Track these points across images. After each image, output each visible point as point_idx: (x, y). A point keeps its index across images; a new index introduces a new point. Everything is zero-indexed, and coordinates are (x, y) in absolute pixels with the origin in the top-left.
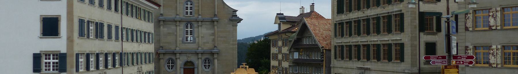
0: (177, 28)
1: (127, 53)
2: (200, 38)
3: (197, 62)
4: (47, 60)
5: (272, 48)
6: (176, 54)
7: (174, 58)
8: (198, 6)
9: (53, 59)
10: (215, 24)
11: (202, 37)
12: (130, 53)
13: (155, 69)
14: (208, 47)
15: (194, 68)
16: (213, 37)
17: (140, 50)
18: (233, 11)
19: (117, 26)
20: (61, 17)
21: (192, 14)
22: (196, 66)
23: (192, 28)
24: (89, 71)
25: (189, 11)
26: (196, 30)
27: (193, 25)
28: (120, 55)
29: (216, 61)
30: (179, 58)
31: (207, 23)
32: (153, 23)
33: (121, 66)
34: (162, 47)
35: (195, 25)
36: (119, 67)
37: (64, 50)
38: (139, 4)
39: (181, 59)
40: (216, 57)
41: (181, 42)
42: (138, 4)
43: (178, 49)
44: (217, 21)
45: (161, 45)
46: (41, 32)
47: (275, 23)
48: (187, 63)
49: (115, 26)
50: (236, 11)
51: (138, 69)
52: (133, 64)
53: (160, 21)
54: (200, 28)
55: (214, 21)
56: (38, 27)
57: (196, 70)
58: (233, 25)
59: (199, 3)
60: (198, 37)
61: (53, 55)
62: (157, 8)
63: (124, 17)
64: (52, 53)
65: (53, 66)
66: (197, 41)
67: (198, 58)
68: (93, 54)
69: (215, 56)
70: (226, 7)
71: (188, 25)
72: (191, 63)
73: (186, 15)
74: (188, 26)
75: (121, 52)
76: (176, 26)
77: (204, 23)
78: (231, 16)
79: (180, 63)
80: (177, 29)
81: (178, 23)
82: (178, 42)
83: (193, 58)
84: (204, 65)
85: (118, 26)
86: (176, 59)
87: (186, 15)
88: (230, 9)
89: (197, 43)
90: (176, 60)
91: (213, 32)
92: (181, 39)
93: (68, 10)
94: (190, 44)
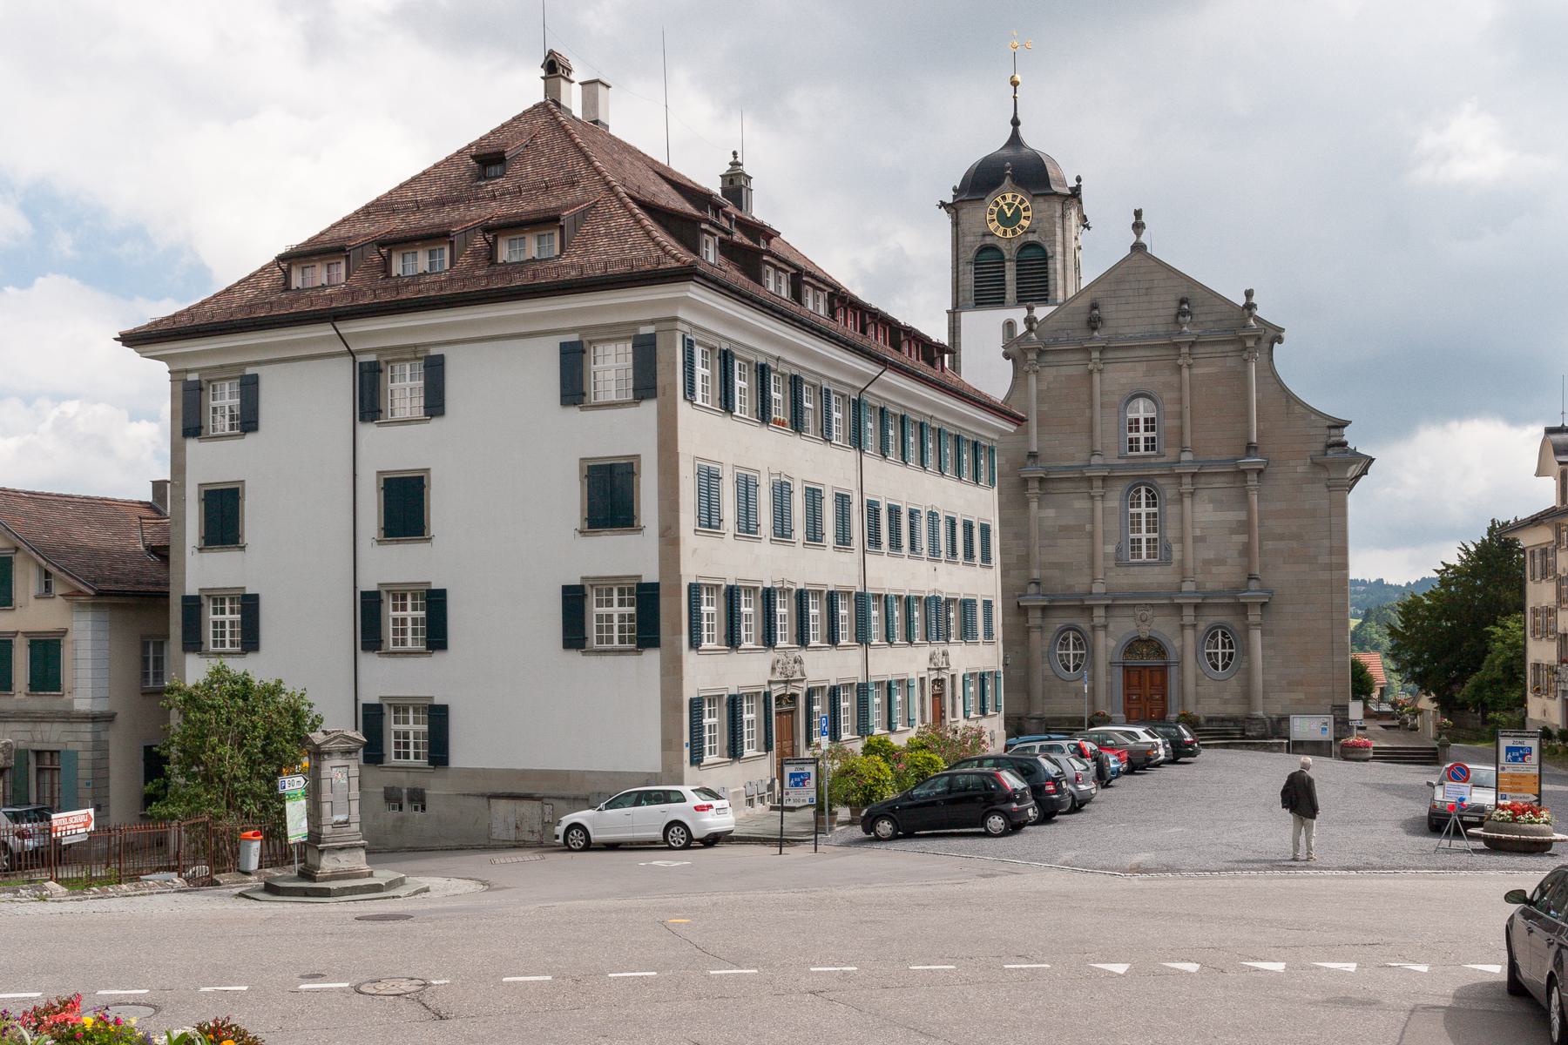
0: (1093, 504)
1: (886, 596)
2: (1189, 541)
3: (1177, 643)
4: (602, 607)
5: (1530, 586)
6: (1091, 608)
7: (1084, 624)
8: (1181, 415)
9: (621, 603)
10: (1250, 483)
11: (1196, 540)
12: (920, 598)
13: (1005, 665)
14: (1224, 575)
15: (1166, 667)
16: (1243, 538)
17: (940, 588)
18: (1330, 427)
19: (843, 496)
20: (639, 462)
21: (1153, 448)
22: (1173, 658)
23: (1154, 505)
24: (737, 648)
25: (1142, 435)
26: (1172, 510)
27: (1157, 490)
28: (856, 600)
29: (1256, 637)
30: (1105, 627)
31: (1219, 482)
32: (996, 488)
33: (862, 644)
34: (1038, 584)
35: (1169, 491)
36: (855, 644)
37: (651, 575)
38: (930, 414)
39: (1111, 628)
40: (1258, 619)
41: (1112, 563)
42: (927, 415)
43: (1098, 588)
44: (1260, 472)
45: (1036, 574)
46: (582, 515)
47: (1540, 472)
48: (1135, 645)
49: (836, 494)
50: (1342, 424)
51: (931, 659)
52: (909, 638)
53: (1026, 481)
54: (1187, 502)
55: (1244, 472)
56: (571, 499)
57: (1173, 672)
58: (1328, 487)
59: (1180, 401)
60: (1181, 540)
61: (621, 592)
62: (1010, 428)
63: (872, 463)
64: (616, 582)
65: (621, 629)
66: (1176, 556)
67: (1183, 627)
68: (752, 592)
69: (1254, 616)
70: (1298, 409)
71: (1139, 491)
72: (1156, 647)
73: (1130, 454)
74: (1139, 498)
75: (859, 589)
76: (1092, 498)
77: (1203, 479)
78: (1321, 447)
79: (1108, 645)
80: (1093, 510)
81: (1098, 490)
82: (1099, 562)
83: (1161, 627)
84: (1209, 654)
85: (848, 496)
86: (1093, 628)
87: (1130, 454)
88: (1313, 417)
89: (1175, 565)
90: (1094, 635)
91: (1242, 516)
92: (1111, 549)
93: (660, 434)
94: (1146, 569)
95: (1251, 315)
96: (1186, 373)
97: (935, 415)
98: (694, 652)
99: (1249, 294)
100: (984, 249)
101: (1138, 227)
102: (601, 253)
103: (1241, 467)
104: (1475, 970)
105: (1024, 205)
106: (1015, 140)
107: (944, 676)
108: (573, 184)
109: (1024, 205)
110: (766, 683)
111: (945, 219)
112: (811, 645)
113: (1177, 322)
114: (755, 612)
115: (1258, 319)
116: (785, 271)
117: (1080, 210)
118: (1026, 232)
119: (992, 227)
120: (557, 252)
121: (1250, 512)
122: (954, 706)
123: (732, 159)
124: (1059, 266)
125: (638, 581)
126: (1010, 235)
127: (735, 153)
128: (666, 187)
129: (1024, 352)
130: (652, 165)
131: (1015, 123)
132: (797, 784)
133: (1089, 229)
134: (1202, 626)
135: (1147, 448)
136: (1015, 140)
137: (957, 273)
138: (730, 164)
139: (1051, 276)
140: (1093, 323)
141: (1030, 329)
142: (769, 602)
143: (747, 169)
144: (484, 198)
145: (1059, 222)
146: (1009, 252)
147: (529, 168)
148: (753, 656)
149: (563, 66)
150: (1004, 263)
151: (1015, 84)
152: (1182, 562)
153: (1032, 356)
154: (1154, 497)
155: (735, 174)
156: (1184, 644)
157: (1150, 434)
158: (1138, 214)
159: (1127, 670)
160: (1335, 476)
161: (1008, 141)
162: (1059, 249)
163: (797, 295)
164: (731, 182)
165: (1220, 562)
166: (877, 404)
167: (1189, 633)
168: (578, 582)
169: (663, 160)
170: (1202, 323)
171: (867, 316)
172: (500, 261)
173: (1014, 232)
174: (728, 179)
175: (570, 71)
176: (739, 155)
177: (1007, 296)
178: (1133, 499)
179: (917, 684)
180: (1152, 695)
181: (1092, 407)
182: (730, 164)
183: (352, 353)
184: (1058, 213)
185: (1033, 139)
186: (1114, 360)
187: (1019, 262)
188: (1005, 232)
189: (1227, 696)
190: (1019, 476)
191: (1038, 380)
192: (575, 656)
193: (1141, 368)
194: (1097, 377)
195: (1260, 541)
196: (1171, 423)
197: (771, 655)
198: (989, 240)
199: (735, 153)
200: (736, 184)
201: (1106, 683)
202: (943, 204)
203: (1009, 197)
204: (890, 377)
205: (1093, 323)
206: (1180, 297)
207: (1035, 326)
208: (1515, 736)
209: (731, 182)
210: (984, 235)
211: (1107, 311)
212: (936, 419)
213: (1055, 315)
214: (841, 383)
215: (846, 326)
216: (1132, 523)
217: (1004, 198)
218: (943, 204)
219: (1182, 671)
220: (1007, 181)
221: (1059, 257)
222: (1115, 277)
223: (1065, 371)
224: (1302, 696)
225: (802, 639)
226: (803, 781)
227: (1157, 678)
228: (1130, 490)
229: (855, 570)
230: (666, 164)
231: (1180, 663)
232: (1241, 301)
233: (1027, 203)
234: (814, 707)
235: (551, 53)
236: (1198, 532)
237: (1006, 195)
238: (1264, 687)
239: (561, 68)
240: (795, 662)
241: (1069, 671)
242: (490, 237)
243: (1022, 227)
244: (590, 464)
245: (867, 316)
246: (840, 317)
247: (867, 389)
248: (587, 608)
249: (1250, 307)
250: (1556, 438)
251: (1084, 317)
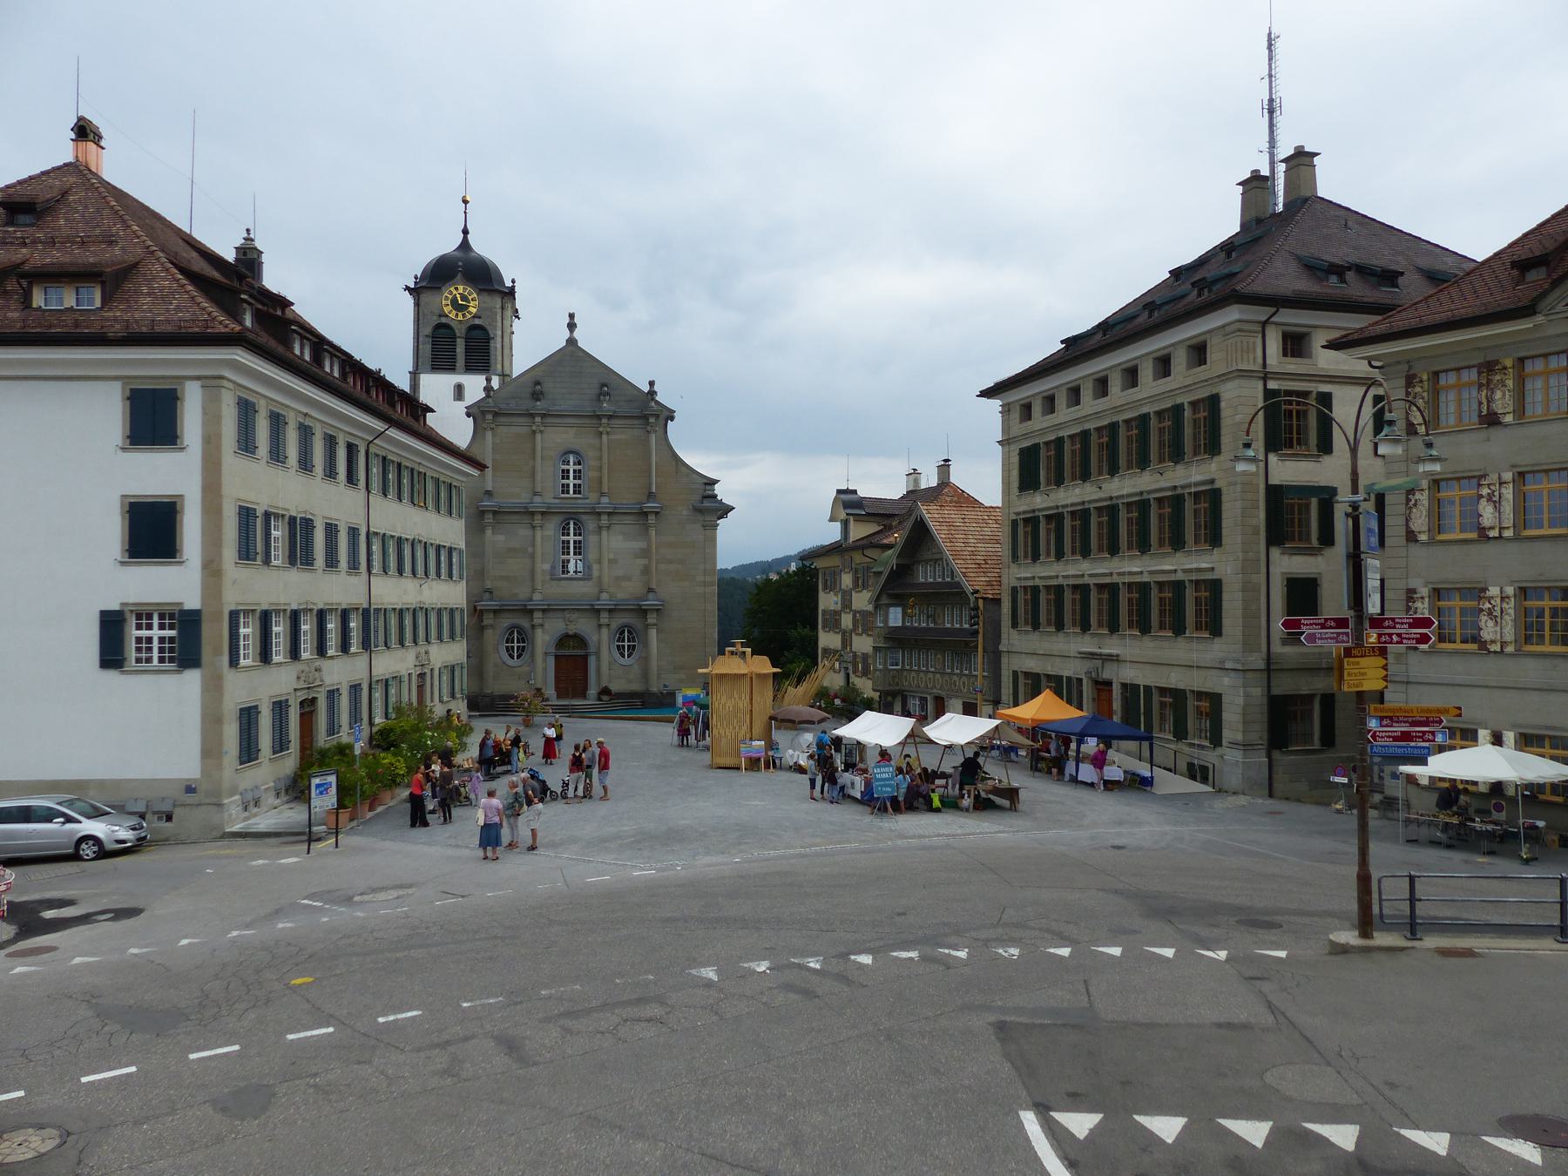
2: (606, 563)
4: (142, 629)
7: (525, 623)
9: (162, 627)
13: (468, 657)
14: (627, 591)
16: (646, 561)
18: (706, 484)
22: (592, 649)
23: (580, 535)
26: (592, 539)
27: (583, 525)
29: (653, 633)
31: (627, 519)
32: (463, 520)
34: (491, 593)
35: (590, 524)
37: (192, 602)
39: (546, 626)
40: (654, 621)
45: (488, 585)
47: (832, 519)
48: (565, 640)
51: (417, 658)
52: (401, 643)
53: (483, 513)
54: (604, 533)
55: (646, 514)
56: (113, 531)
57: (592, 660)
58: (704, 526)
59: (601, 459)
60: (599, 561)
61: (162, 617)
63: (376, 500)
65: (161, 650)
66: (595, 573)
67: (600, 626)
69: (652, 619)
70: (684, 470)
71: (569, 524)
72: (579, 640)
73: (563, 496)
74: (569, 529)
75: (365, 606)
76: (534, 527)
79: (544, 638)
80: (534, 537)
81: (538, 520)
82: (539, 577)
83: (583, 626)
84: (618, 646)
85: (358, 529)
86: (533, 627)
87: (563, 496)
88: (694, 476)
90: (533, 633)
91: (642, 545)
92: (547, 567)
93: (204, 479)
95: (653, 399)
96: (604, 437)
97: (423, 463)
98: (233, 670)
99: (652, 384)
100: (439, 326)
101: (572, 326)
102: (145, 310)
103: (645, 510)
104: (949, 955)
105: (472, 296)
106: (465, 245)
107: (426, 671)
108: (111, 243)
109: (472, 296)
110: (293, 691)
111: (408, 301)
112: (328, 655)
113: (599, 400)
114: (284, 631)
115: (658, 403)
116: (308, 339)
117: (514, 304)
118: (473, 317)
119: (446, 310)
120: (98, 304)
121: (649, 542)
122: (432, 693)
123: (246, 235)
124: (499, 346)
125: (179, 608)
126: (460, 318)
128: (194, 254)
129: (483, 413)
130: (178, 232)
131: (465, 232)
132: (321, 793)
133: (519, 319)
134: (615, 625)
135: (575, 492)
136: (465, 245)
137: (418, 343)
138: (244, 239)
139: (492, 353)
141: (488, 396)
142: (296, 621)
143: (259, 244)
144: (12, 243)
145: (499, 311)
146: (460, 331)
147: (62, 222)
148: (283, 669)
149: (94, 133)
150: (455, 338)
151: (465, 202)
152: (600, 578)
153: (489, 417)
154: (579, 528)
155: (249, 248)
156: (602, 640)
157: (577, 482)
158: (572, 316)
159: (557, 657)
160: (708, 519)
162: (499, 333)
163: (317, 359)
164: (245, 254)
165: (628, 578)
166: (381, 453)
167: (605, 631)
168: (117, 608)
169: (186, 229)
171: (370, 380)
172: (34, 306)
173: (464, 315)
174: (243, 251)
175: (100, 137)
176: (252, 232)
177: (458, 365)
179: (406, 679)
181: (534, 458)
182: (244, 239)
184: (499, 306)
185: (482, 247)
187: (467, 339)
188: (457, 315)
190: (478, 508)
191: (493, 436)
192: (112, 676)
193: (572, 431)
194: (538, 436)
195: (657, 564)
196: (593, 474)
197: (298, 666)
198: (444, 320)
199: (248, 230)
201: (544, 671)
202: (407, 288)
203: (459, 289)
204: (393, 433)
205: (537, 396)
207: (492, 393)
209: (245, 254)
210: (440, 316)
211: (548, 386)
212: (310, 416)
214: (354, 435)
215: (353, 385)
216: (563, 548)
217: (456, 289)
218: (407, 288)
219: (598, 659)
220: (459, 275)
221: (499, 339)
222: (553, 363)
223: (514, 430)
224: (684, 677)
225: (321, 650)
228: (563, 522)
229: (364, 589)
230: (189, 232)
231: (598, 654)
232: (646, 389)
235: (81, 119)
236: (612, 556)
238: (658, 670)
239: (92, 134)
240: (316, 670)
241: (513, 659)
242: (25, 284)
243: (470, 313)
244: (133, 501)
245: (370, 380)
246: (351, 380)
248: (127, 629)
249: (652, 393)
250: (843, 497)
251: (530, 390)
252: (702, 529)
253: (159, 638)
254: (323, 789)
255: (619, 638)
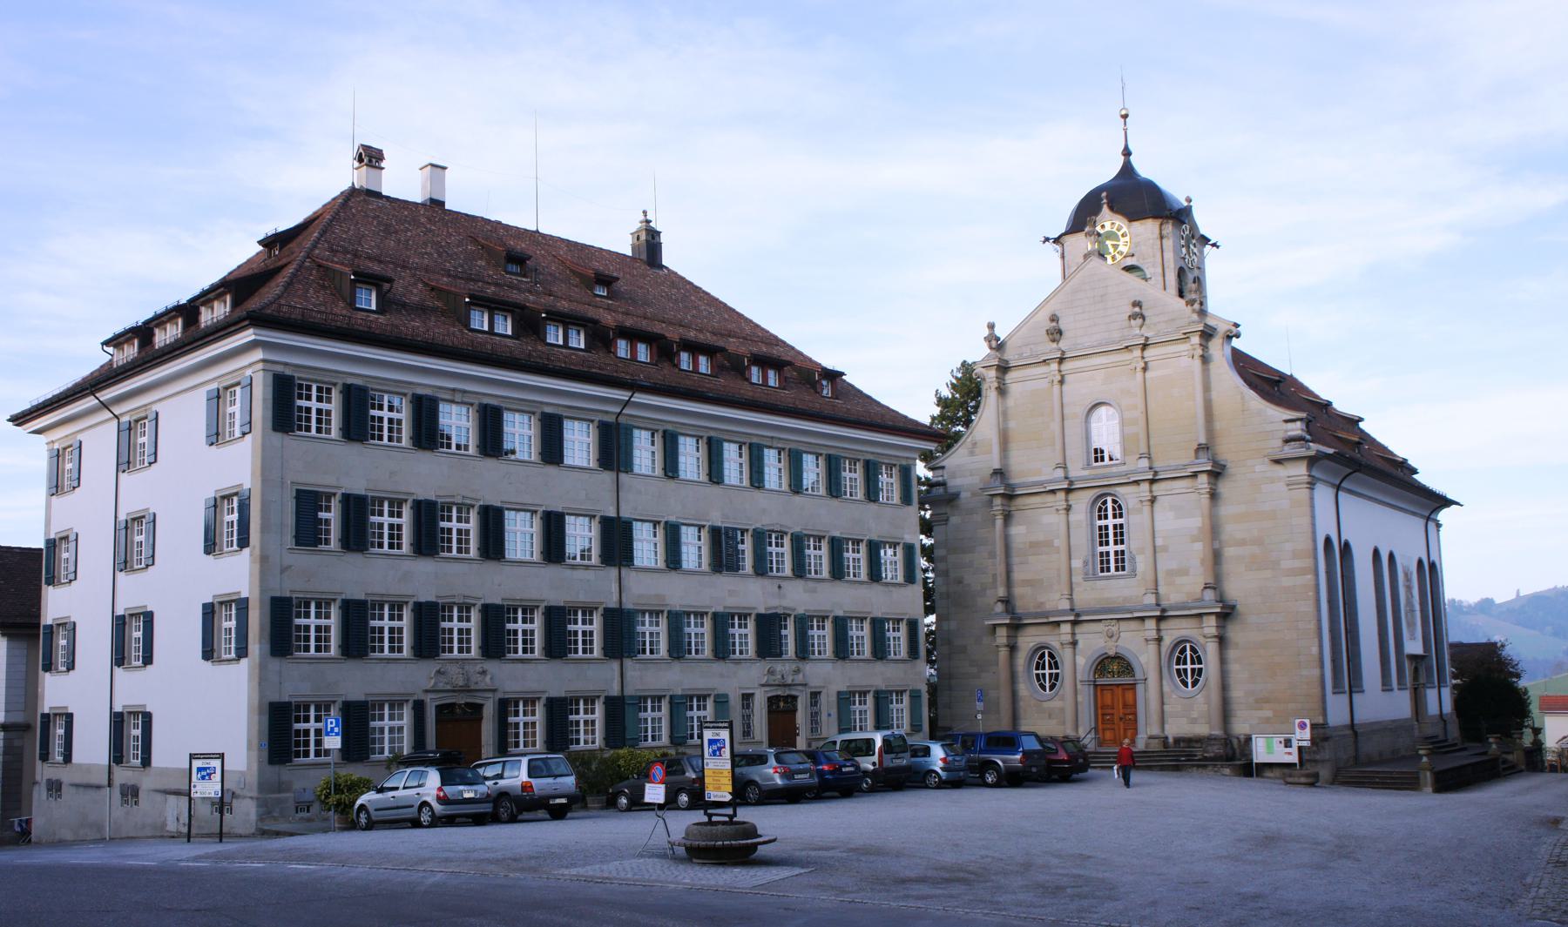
22: (1139, 675)
71: (1105, 503)
74: (1106, 510)
106: (1127, 170)
127: (645, 213)
131: (1127, 153)
132: (203, 778)
136: (1127, 170)
140: (1056, 334)
161: (1116, 177)
165: (1183, 572)
170: (1155, 324)
174: (636, 235)
178: (1100, 510)
180: (1125, 714)
183: (116, 416)
185: (1144, 169)
186: (1073, 371)
189: (1195, 715)
199: (645, 213)
200: (650, 243)
204: (640, 398)
206: (1132, 301)
208: (714, 727)
213: (1018, 331)
216: (1101, 536)
220: (1105, 209)
226: (209, 775)
227: (1129, 695)
233: (1125, 229)
234: (509, 718)
237: (1105, 223)
241: (1045, 690)
247: (624, 411)
252: (1286, 488)
253: (316, 626)
254: (205, 773)
255: (1179, 658)
